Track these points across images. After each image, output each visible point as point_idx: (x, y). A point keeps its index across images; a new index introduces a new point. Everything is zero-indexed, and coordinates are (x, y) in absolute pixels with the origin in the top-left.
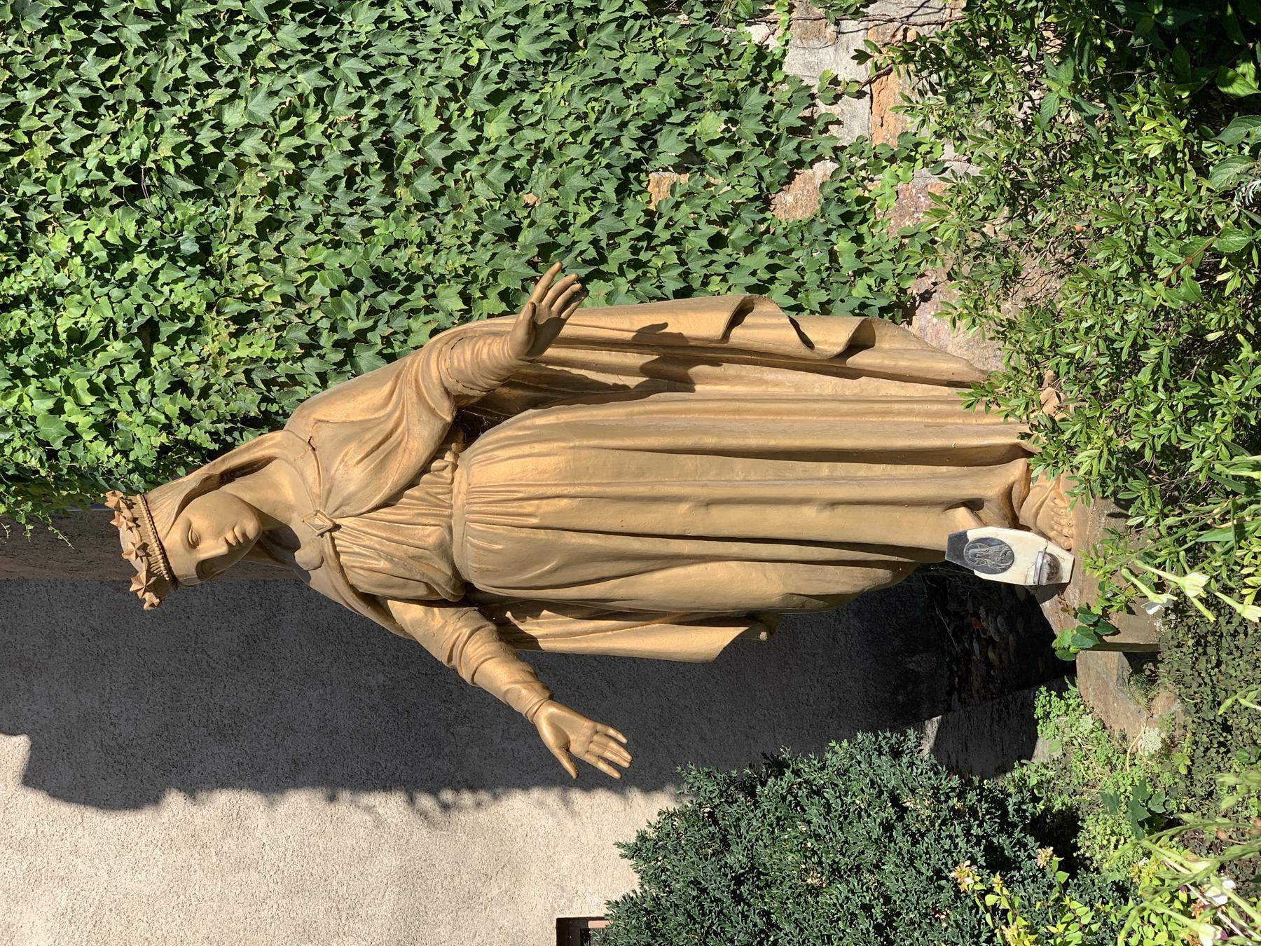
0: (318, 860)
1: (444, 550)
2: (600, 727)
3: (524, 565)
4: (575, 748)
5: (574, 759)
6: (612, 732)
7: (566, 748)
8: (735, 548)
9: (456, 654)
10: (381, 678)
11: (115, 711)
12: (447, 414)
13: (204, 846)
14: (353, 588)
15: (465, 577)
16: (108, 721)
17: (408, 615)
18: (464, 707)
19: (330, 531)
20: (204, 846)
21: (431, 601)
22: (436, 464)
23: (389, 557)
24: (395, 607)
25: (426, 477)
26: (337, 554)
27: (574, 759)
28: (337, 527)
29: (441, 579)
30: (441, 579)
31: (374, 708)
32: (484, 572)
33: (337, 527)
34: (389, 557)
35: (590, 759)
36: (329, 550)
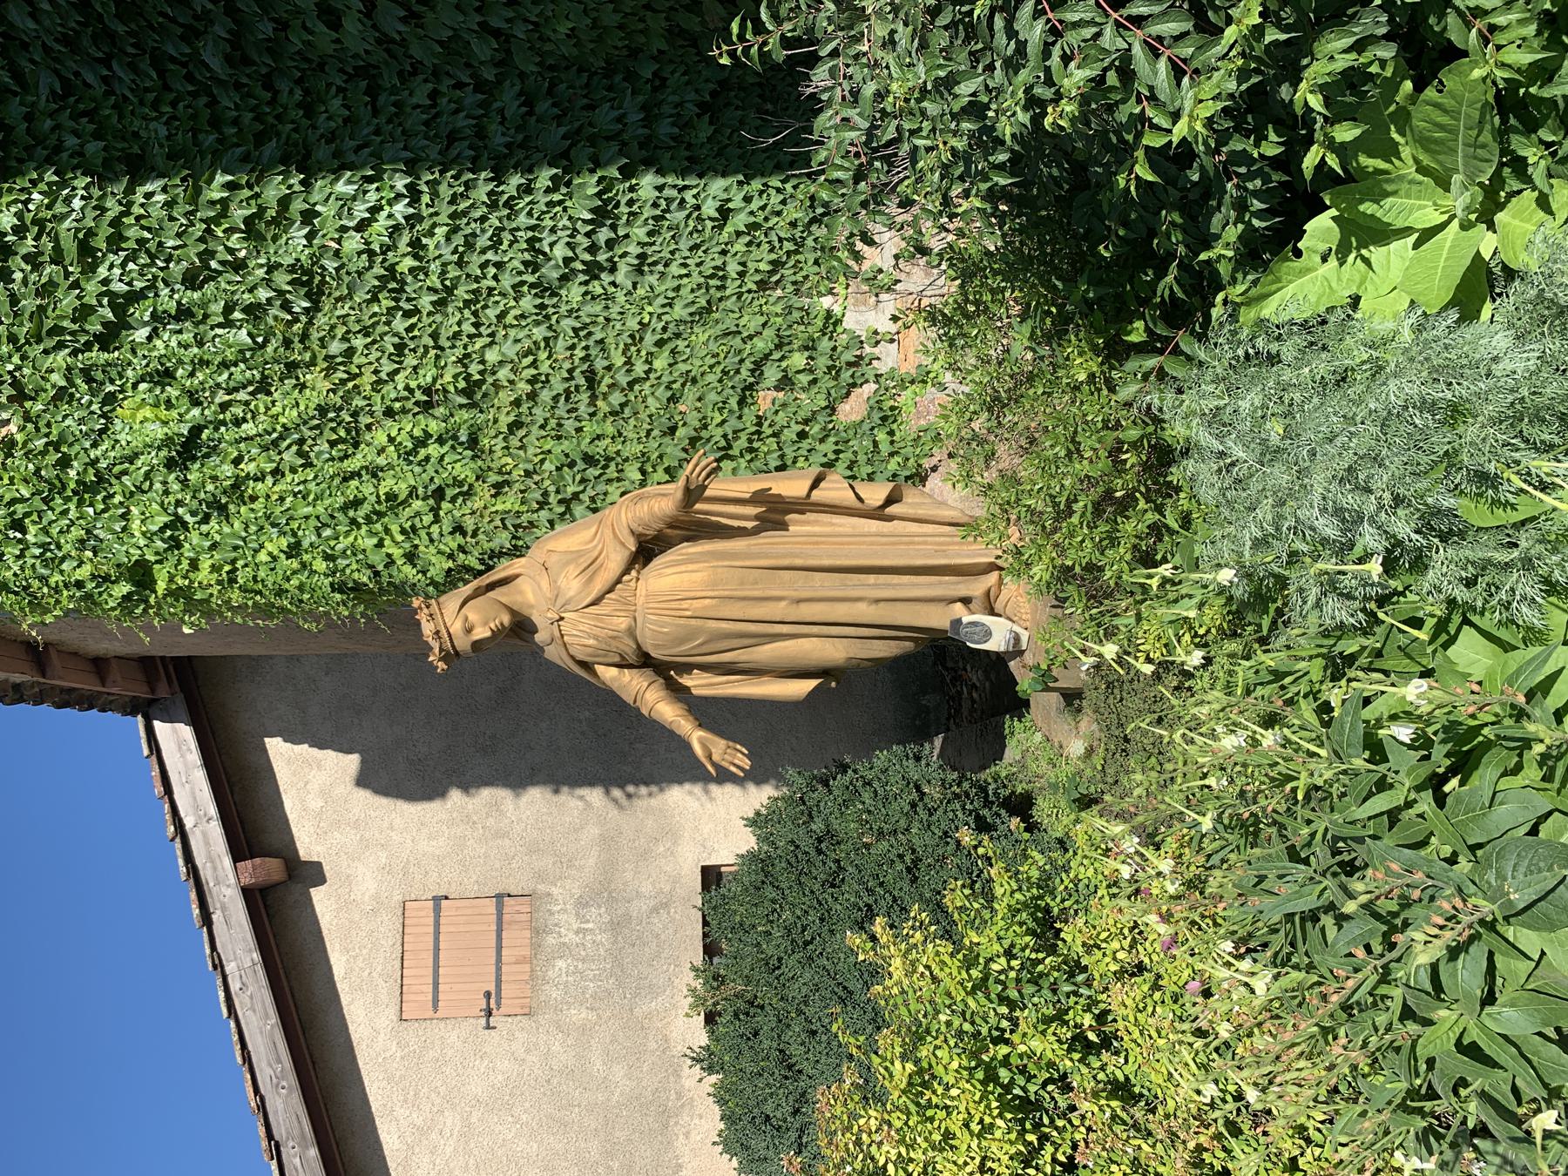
1: (631, 632)
3: (682, 641)
4: (716, 757)
5: (714, 764)
7: (710, 757)
14: (572, 657)
17: (608, 674)
22: (626, 578)
23: (596, 638)
24: (599, 669)
27: (714, 764)
28: (562, 619)
29: (629, 651)
30: (629, 651)
31: (583, 733)
32: (657, 646)
34: (596, 638)
36: (557, 634)
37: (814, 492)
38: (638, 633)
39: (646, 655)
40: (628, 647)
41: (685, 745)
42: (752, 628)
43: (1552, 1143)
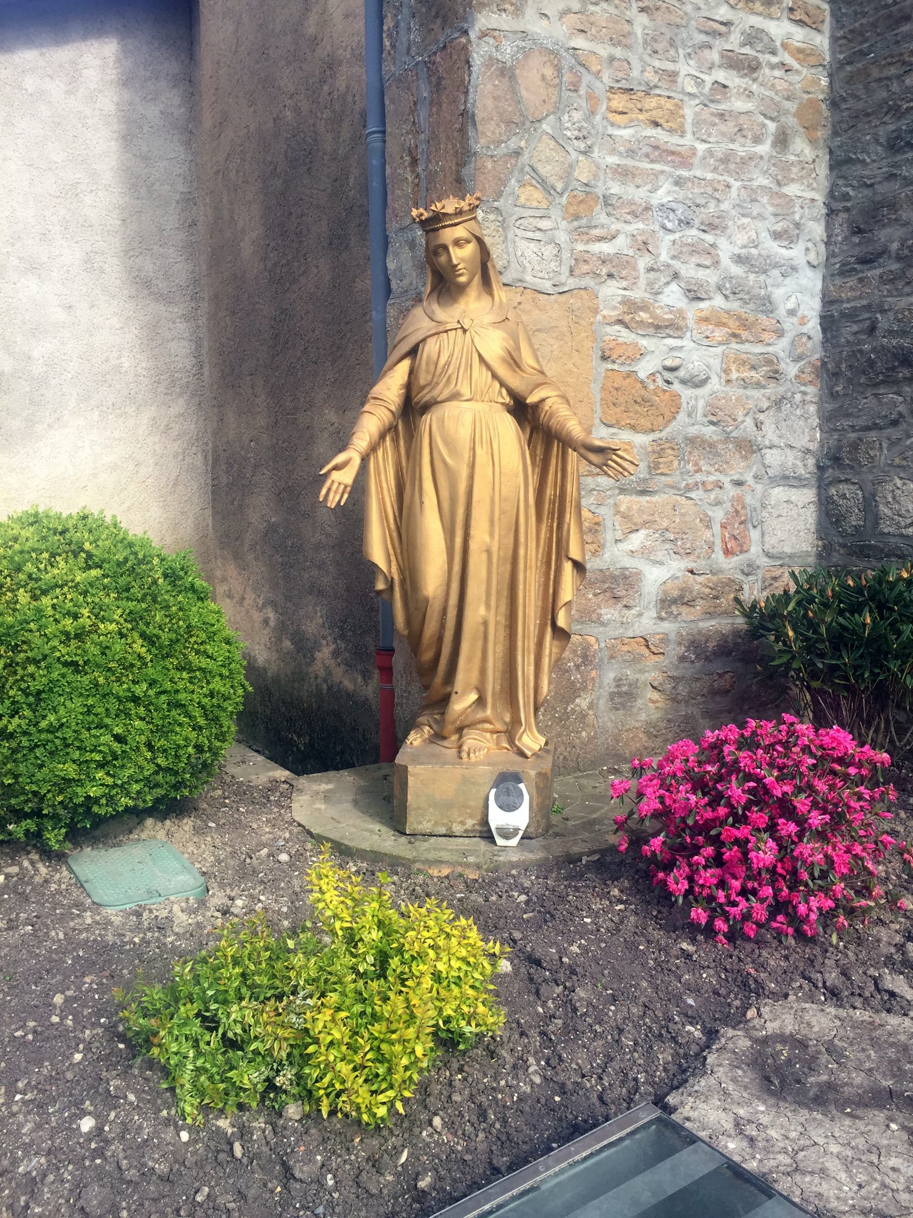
0: (6, 319)
1: (455, 396)
2: (349, 489)
3: (447, 443)
4: (335, 475)
5: (330, 472)
6: (346, 496)
7: (337, 468)
8: (457, 568)
9: (378, 402)
10: (126, 365)
11: (100, 194)
12: (531, 399)
13: (13, 245)
14: (424, 340)
15: (433, 409)
16: (94, 188)
17: (399, 374)
18: (110, 417)
19: (462, 327)
20: (13, 245)
21: (409, 387)
22: (504, 391)
23: (448, 364)
24: (405, 365)
25: (497, 385)
26: (446, 331)
27: (330, 472)
28: (465, 331)
29: (435, 393)
30: (435, 393)
31: (107, 360)
32: (442, 421)
33: (465, 331)
34: (448, 364)
35: (328, 484)
36: (449, 327)
37: (570, 563)
38: (454, 403)
39: (426, 408)
40: (425, 396)
41: (343, 446)
42: (461, 511)
43: (756, 523)
